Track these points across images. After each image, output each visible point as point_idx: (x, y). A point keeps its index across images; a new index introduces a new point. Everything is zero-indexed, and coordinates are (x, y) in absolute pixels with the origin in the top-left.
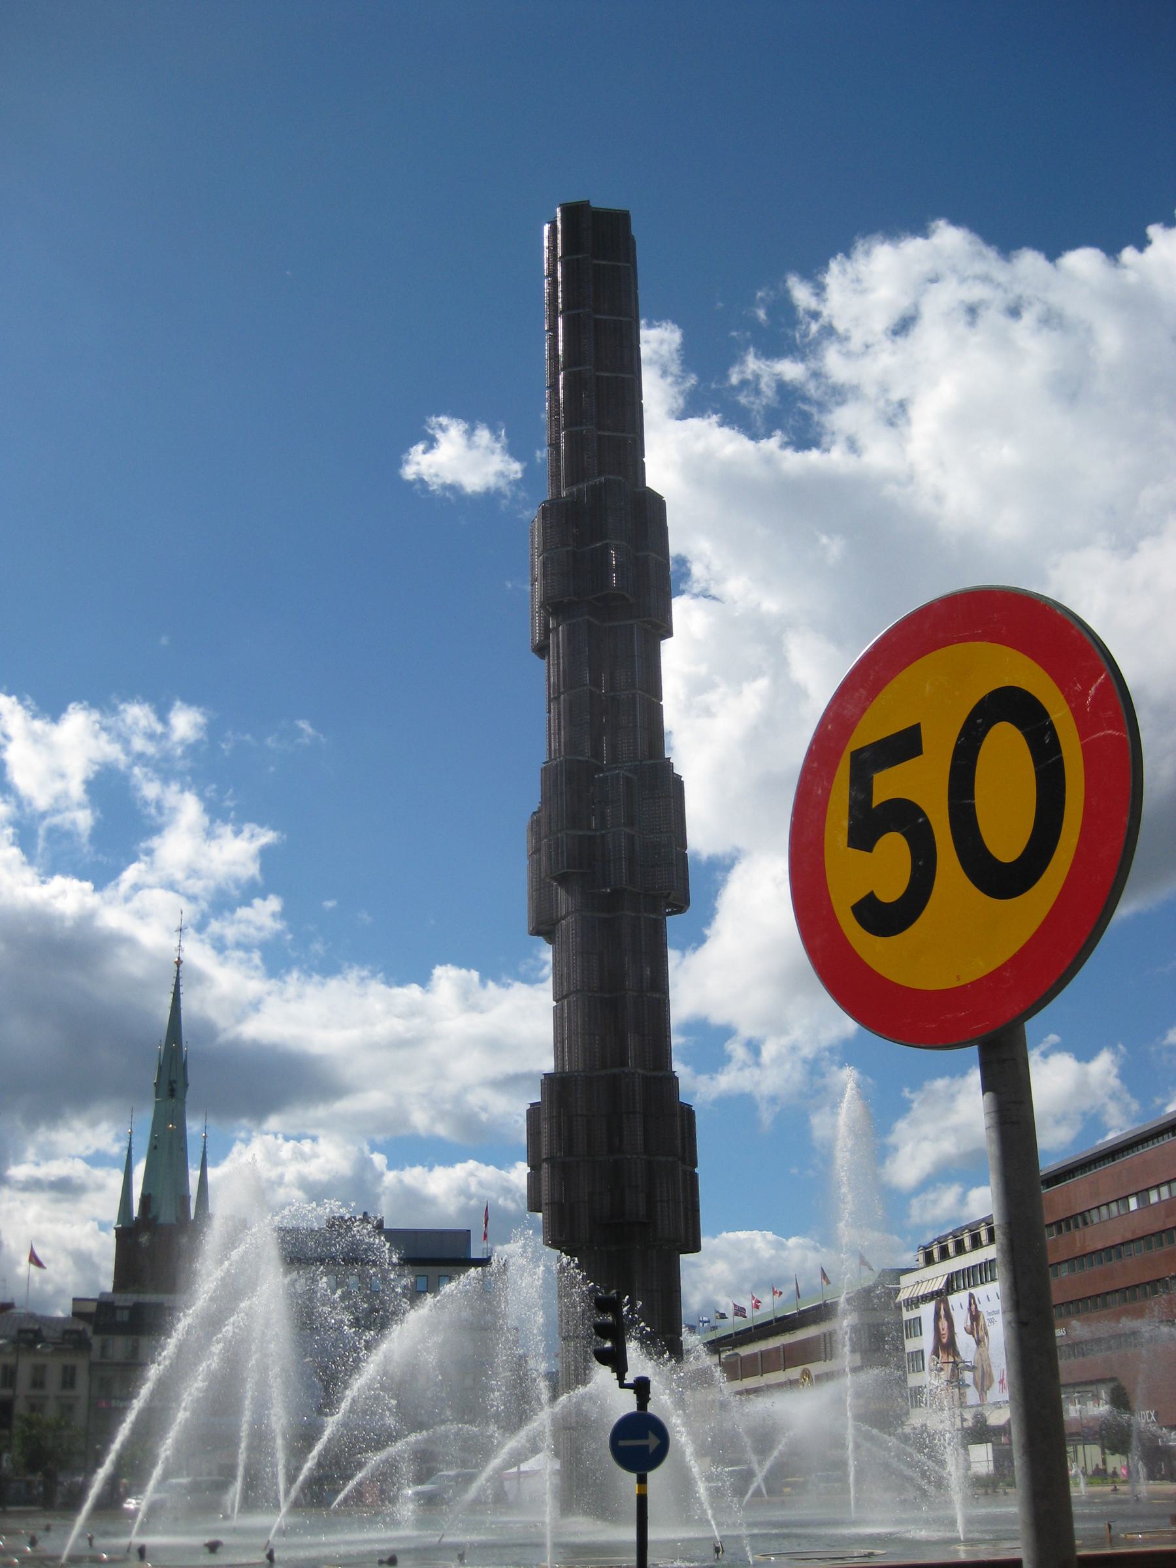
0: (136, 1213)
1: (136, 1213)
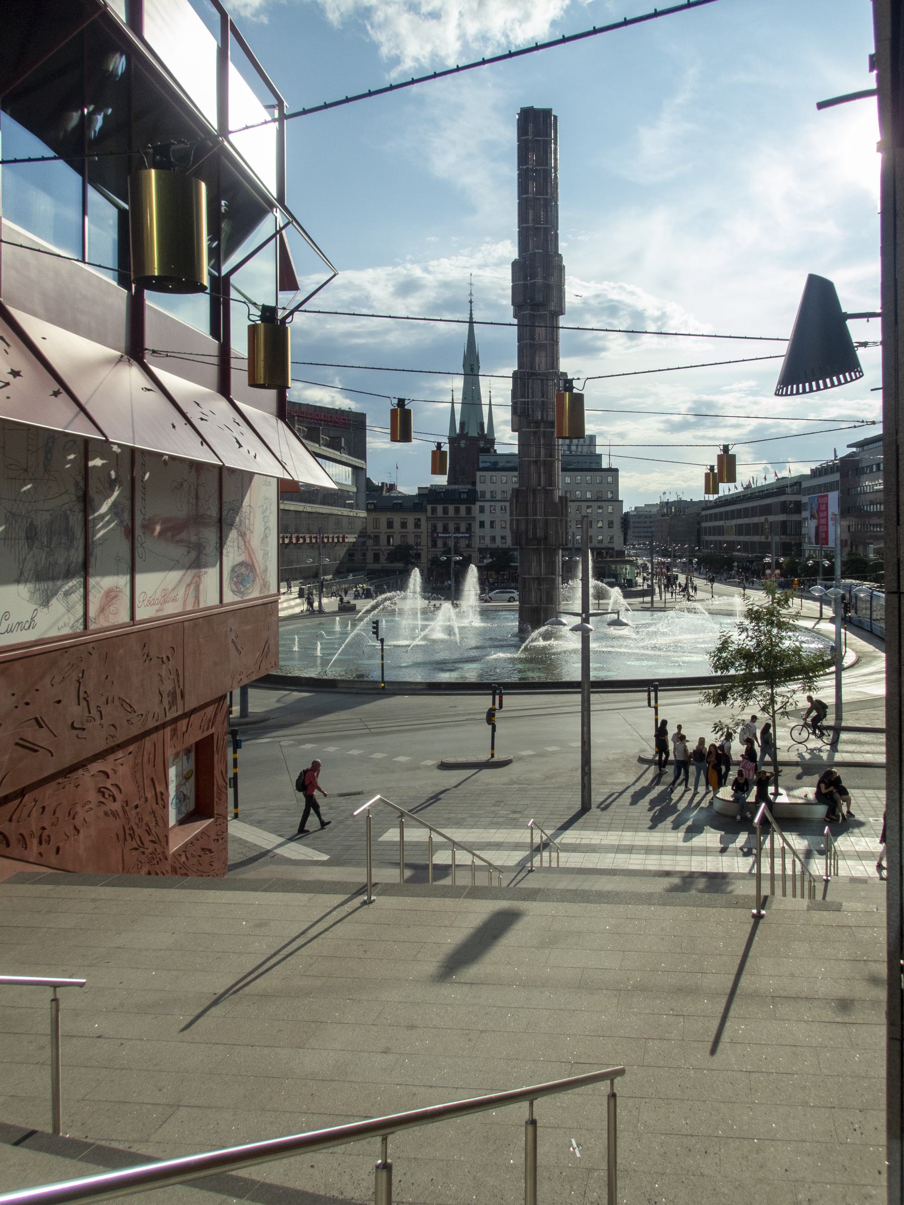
0: (458, 431)
1: (458, 431)
